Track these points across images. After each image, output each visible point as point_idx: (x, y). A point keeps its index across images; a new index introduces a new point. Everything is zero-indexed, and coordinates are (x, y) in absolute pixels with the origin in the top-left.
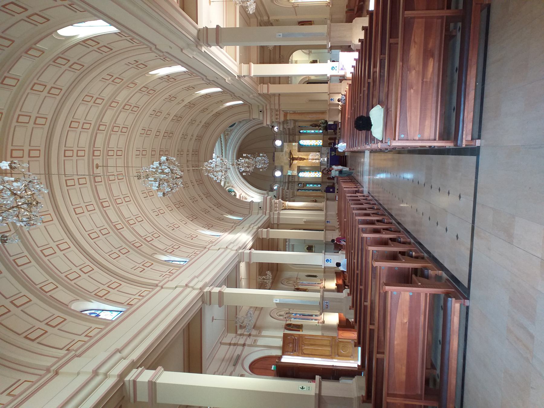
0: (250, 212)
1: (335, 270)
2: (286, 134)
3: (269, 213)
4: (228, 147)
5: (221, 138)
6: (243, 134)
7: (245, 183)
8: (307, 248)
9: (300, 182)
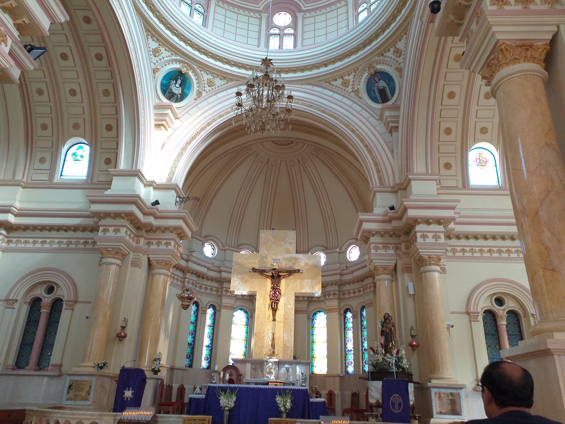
2: (341, 275)
6: (347, 126)
9: (219, 311)
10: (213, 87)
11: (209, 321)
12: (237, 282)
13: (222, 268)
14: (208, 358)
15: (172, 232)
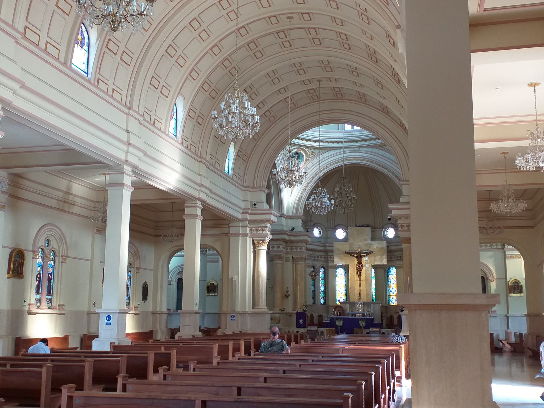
0: (247, 189)
1: (157, 332)
3: (245, 220)
4: (370, 149)
5: (375, 139)
6: (393, 174)
7: (314, 180)
8: (213, 284)
9: (328, 270)
10: (314, 155)
11: (322, 276)
12: (337, 260)
13: (327, 245)
14: (324, 298)
15: (302, 242)
